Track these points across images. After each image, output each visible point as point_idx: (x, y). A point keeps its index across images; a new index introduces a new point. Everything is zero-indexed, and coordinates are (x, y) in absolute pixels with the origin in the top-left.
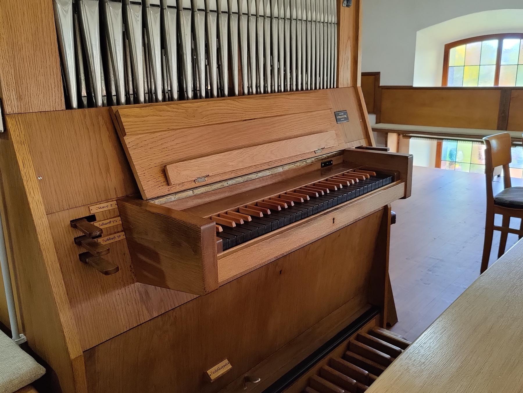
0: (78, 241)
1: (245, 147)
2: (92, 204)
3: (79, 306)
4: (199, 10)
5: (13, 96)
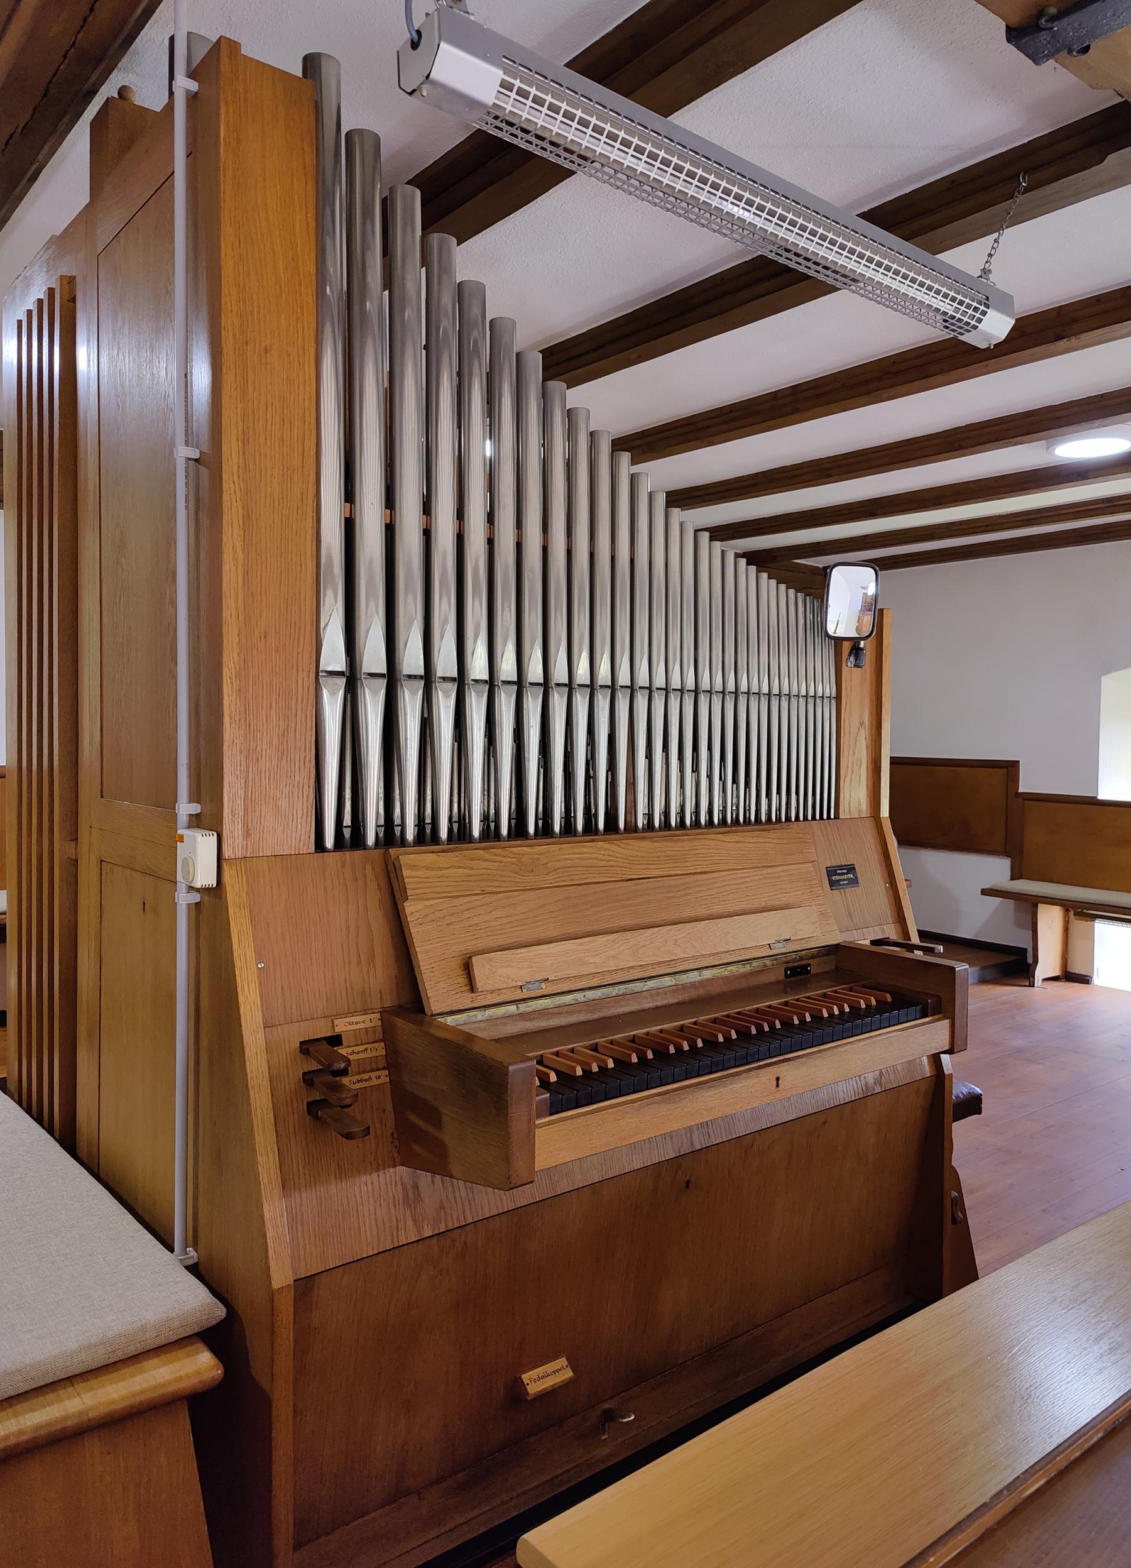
0: (308, 1079)
1: (624, 930)
2: (339, 1016)
3: (298, 1197)
4: (558, 685)
5: (239, 829)
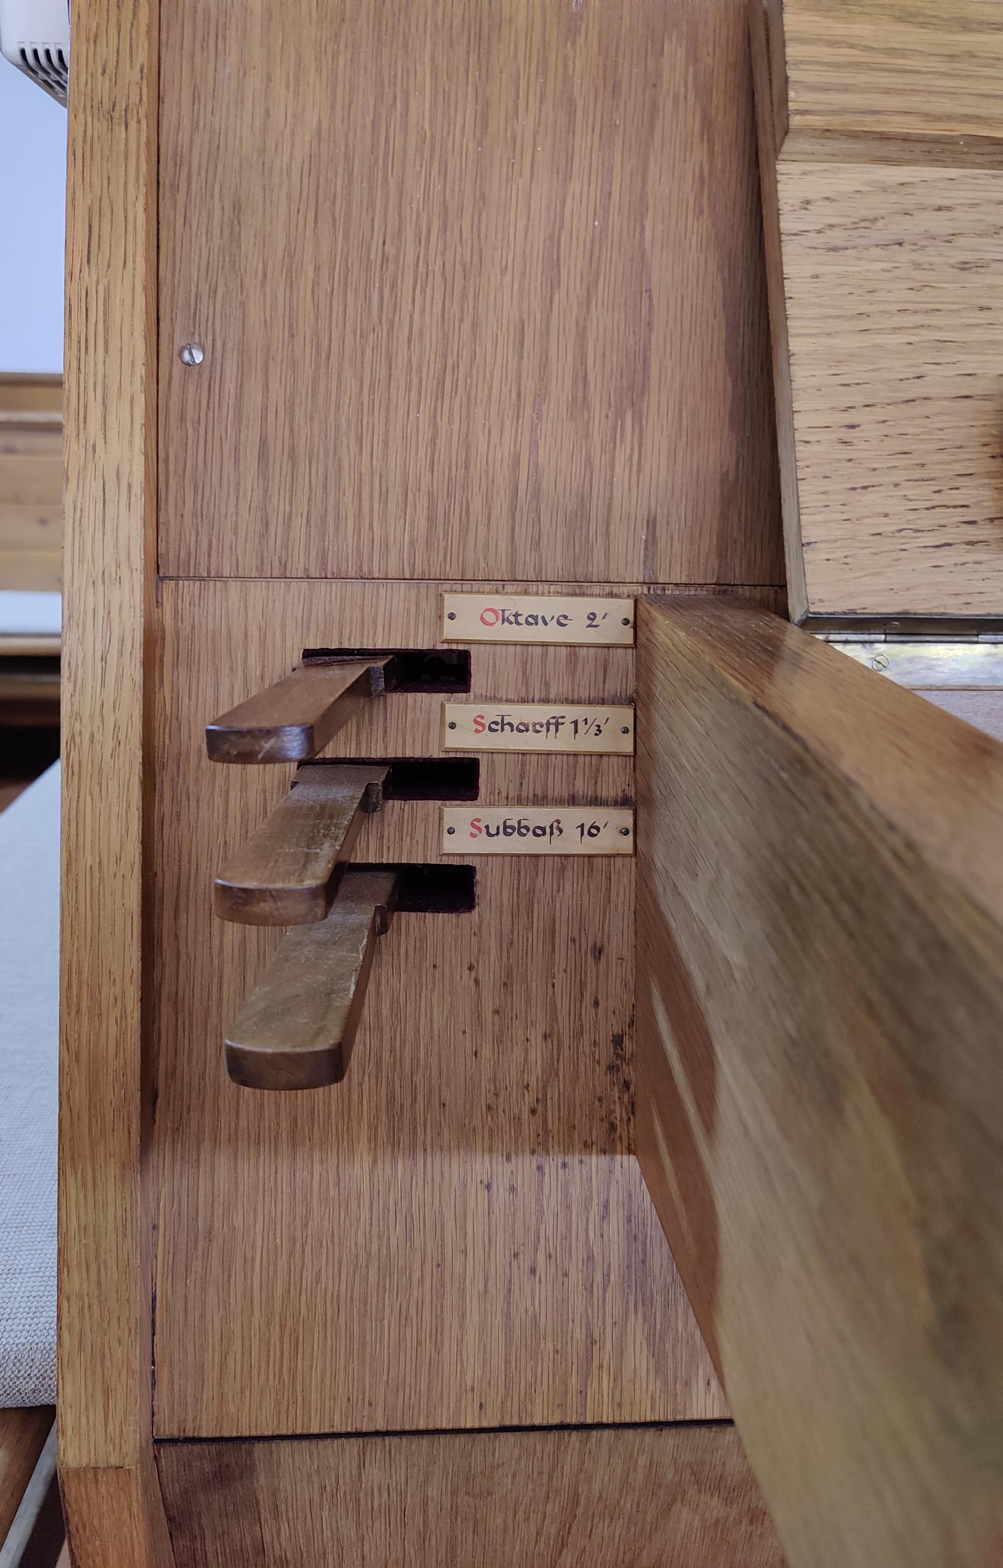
2: (465, 581)
